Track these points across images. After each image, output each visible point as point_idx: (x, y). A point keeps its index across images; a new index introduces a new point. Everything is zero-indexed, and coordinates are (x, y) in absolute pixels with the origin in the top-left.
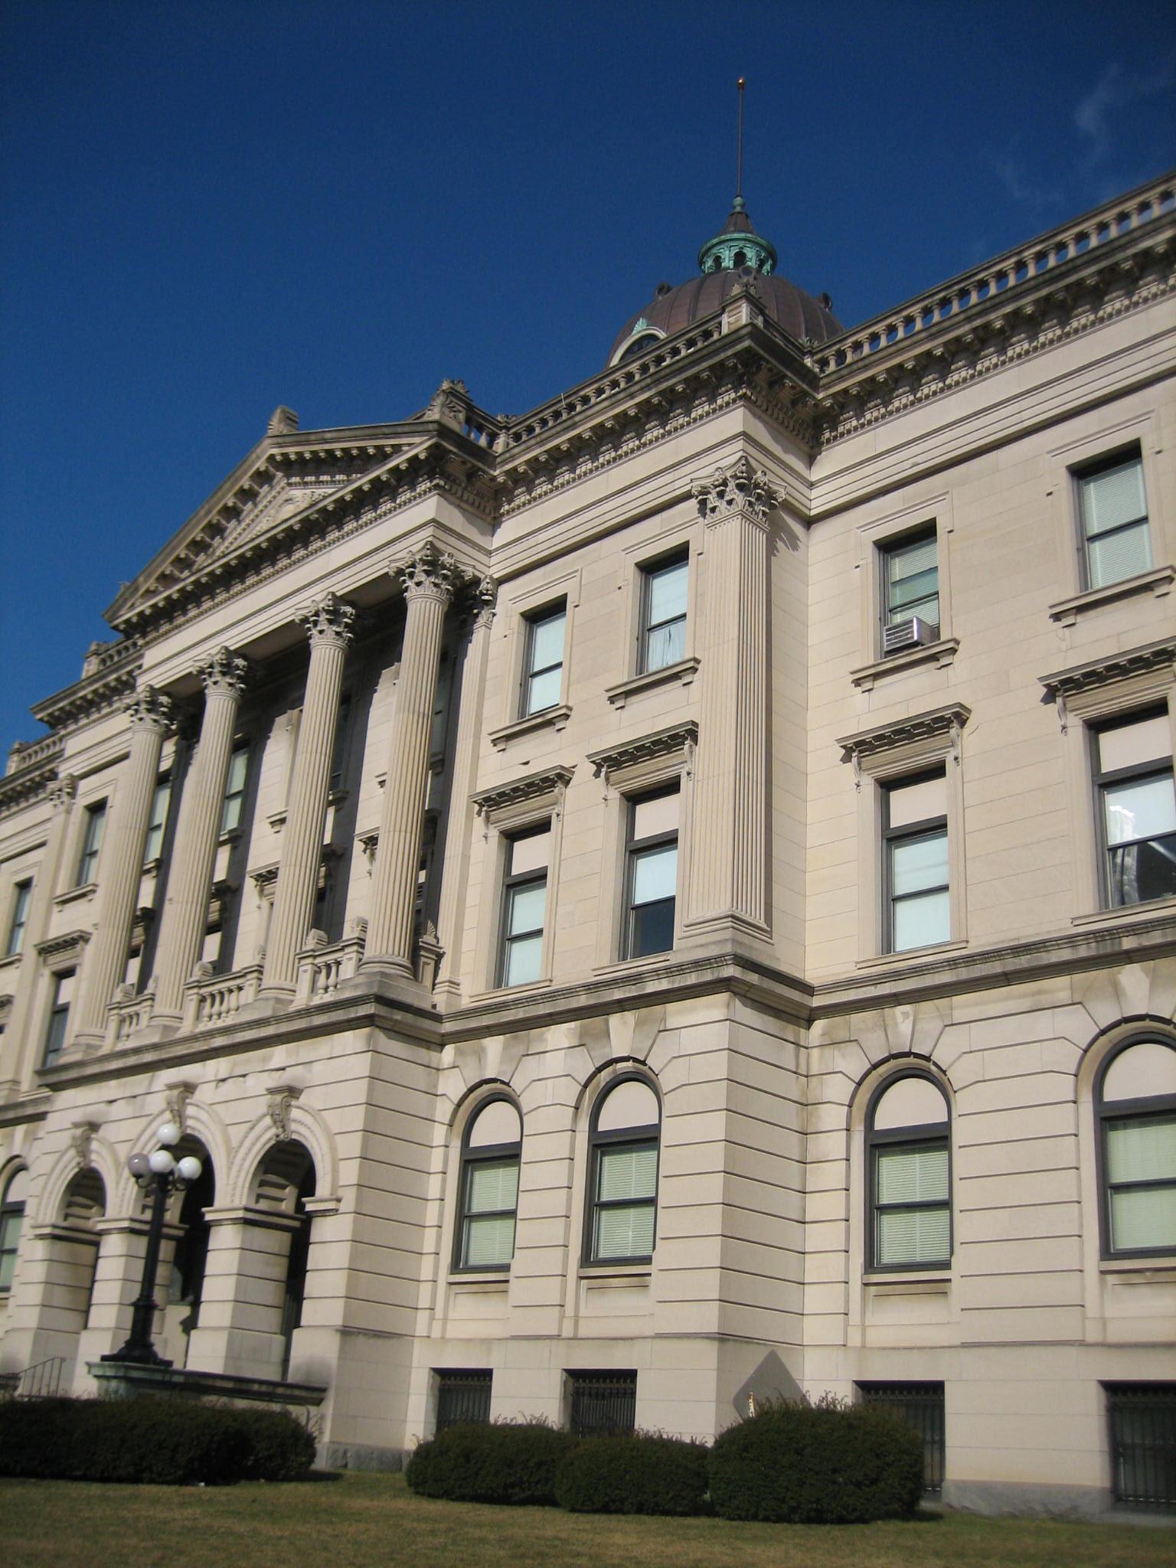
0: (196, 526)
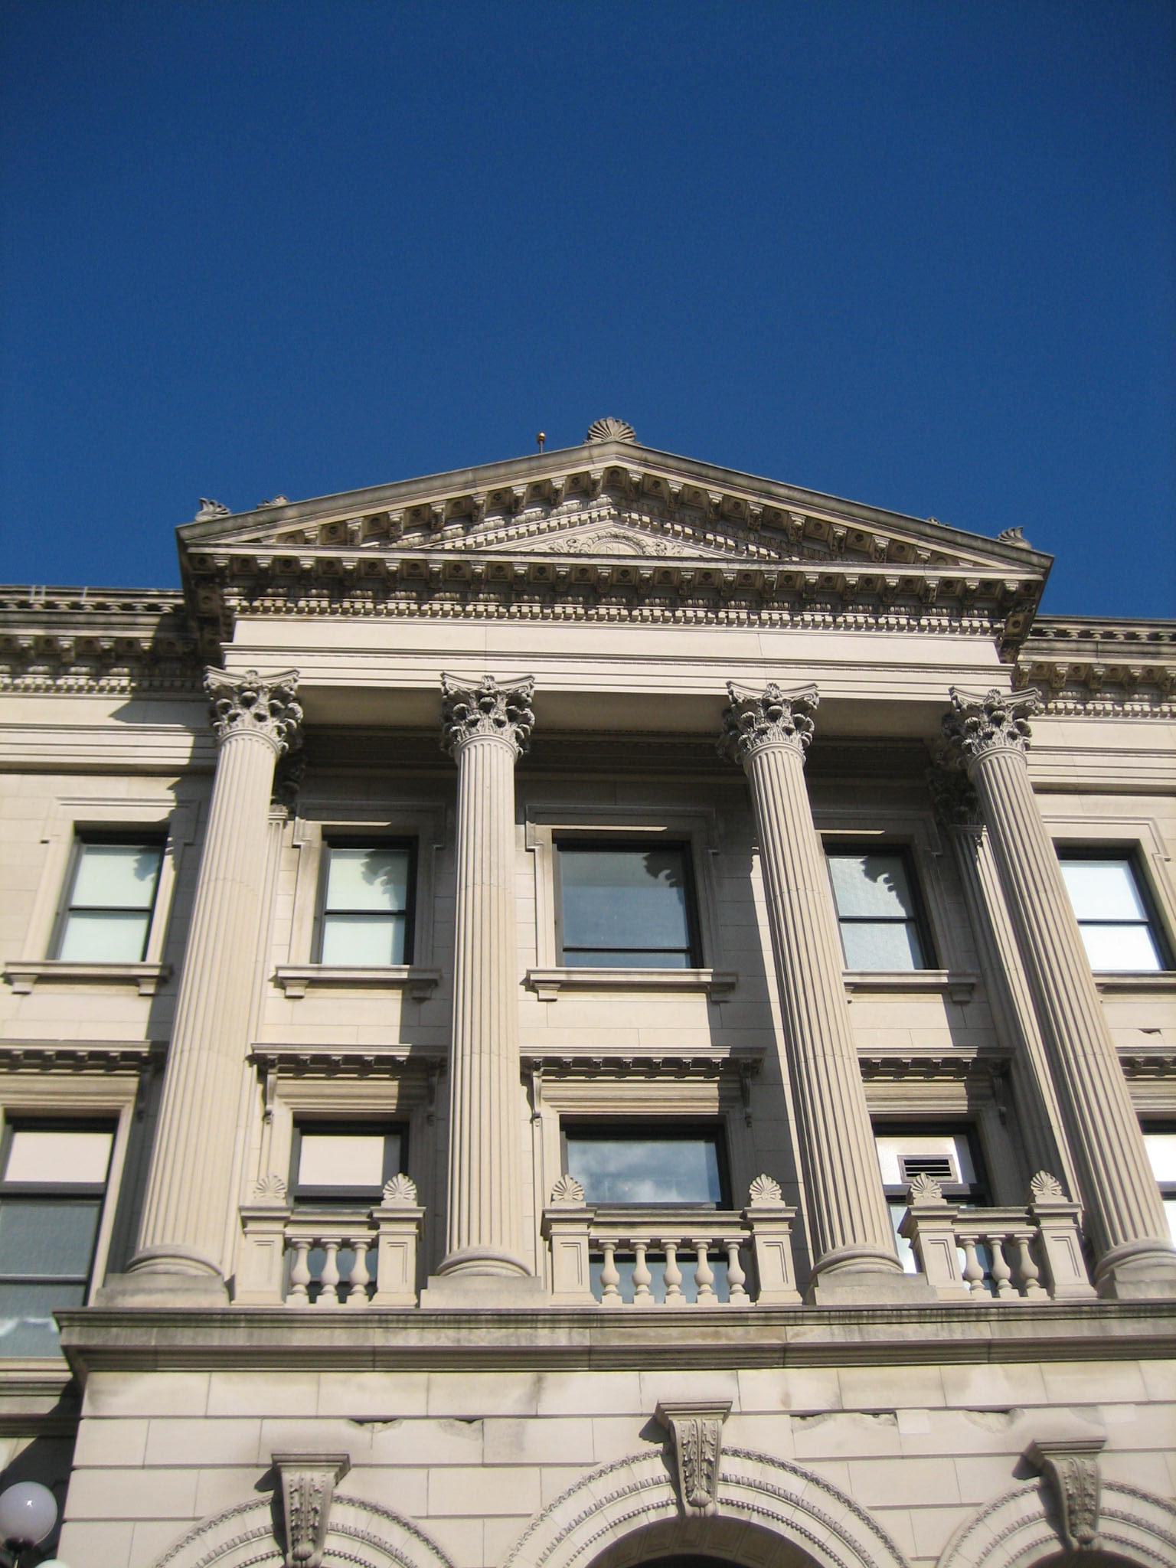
0: (445, 489)
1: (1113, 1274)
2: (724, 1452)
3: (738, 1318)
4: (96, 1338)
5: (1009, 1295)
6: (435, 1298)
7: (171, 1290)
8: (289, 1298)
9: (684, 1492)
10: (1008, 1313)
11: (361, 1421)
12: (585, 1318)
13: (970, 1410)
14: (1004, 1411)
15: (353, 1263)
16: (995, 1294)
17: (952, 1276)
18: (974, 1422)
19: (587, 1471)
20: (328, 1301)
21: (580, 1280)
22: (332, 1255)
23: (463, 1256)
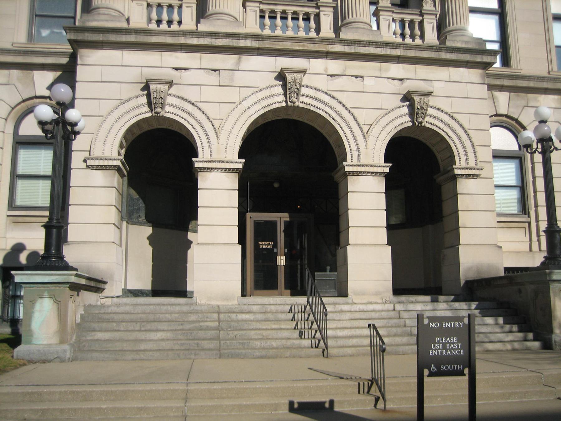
1: (446, 36)
2: (303, 86)
3: (312, 40)
4: (80, 37)
5: (408, 40)
6: (203, 27)
7: (107, 21)
8: (150, 25)
9: (288, 98)
10: (407, 47)
11: (177, 69)
12: (257, 37)
13: (389, 78)
14: (401, 80)
15: (173, 12)
16: (404, 40)
17: (389, 32)
18: (389, 82)
19: (255, 90)
20: (164, 26)
21: (256, 23)
22: (165, 10)
23: (213, 12)
